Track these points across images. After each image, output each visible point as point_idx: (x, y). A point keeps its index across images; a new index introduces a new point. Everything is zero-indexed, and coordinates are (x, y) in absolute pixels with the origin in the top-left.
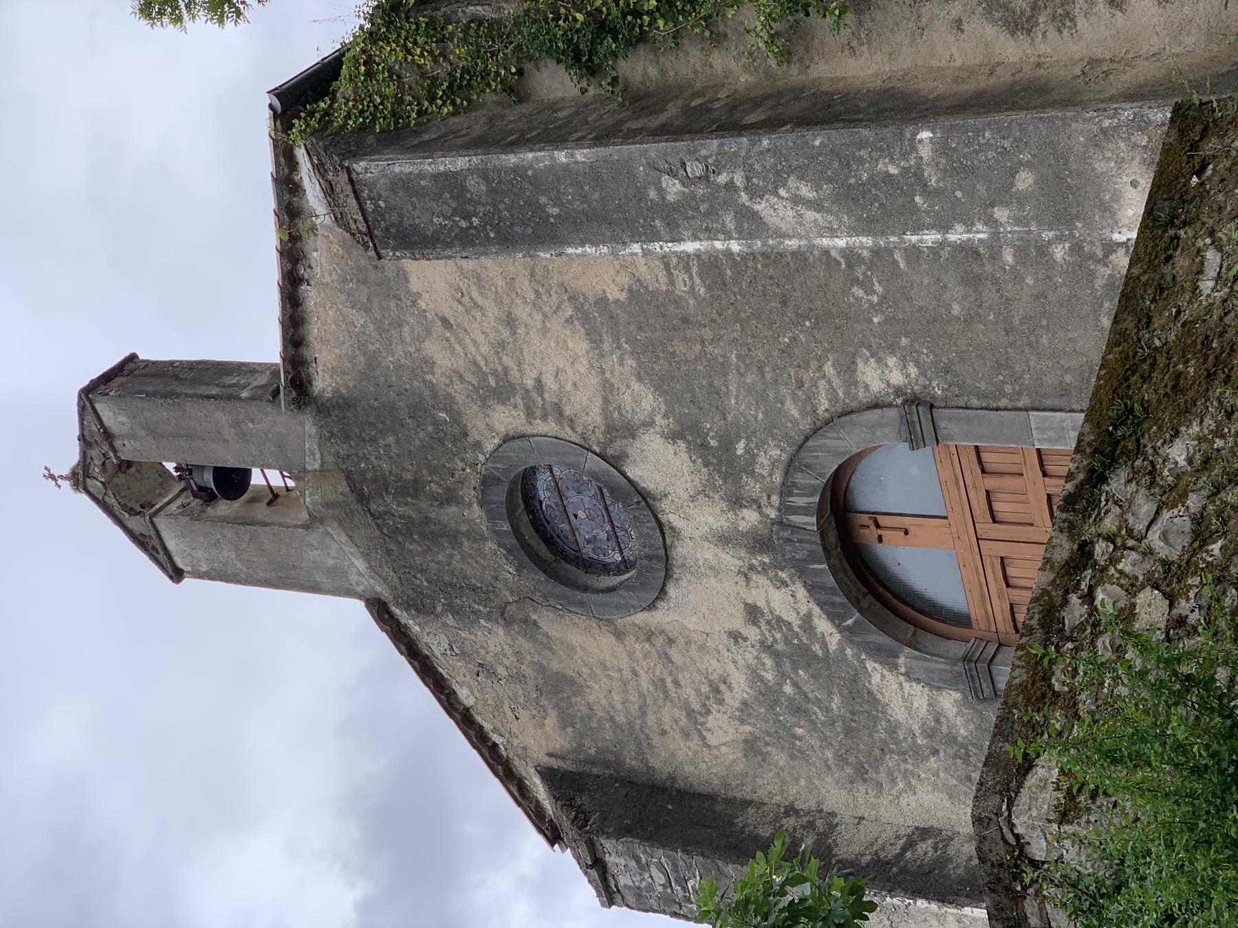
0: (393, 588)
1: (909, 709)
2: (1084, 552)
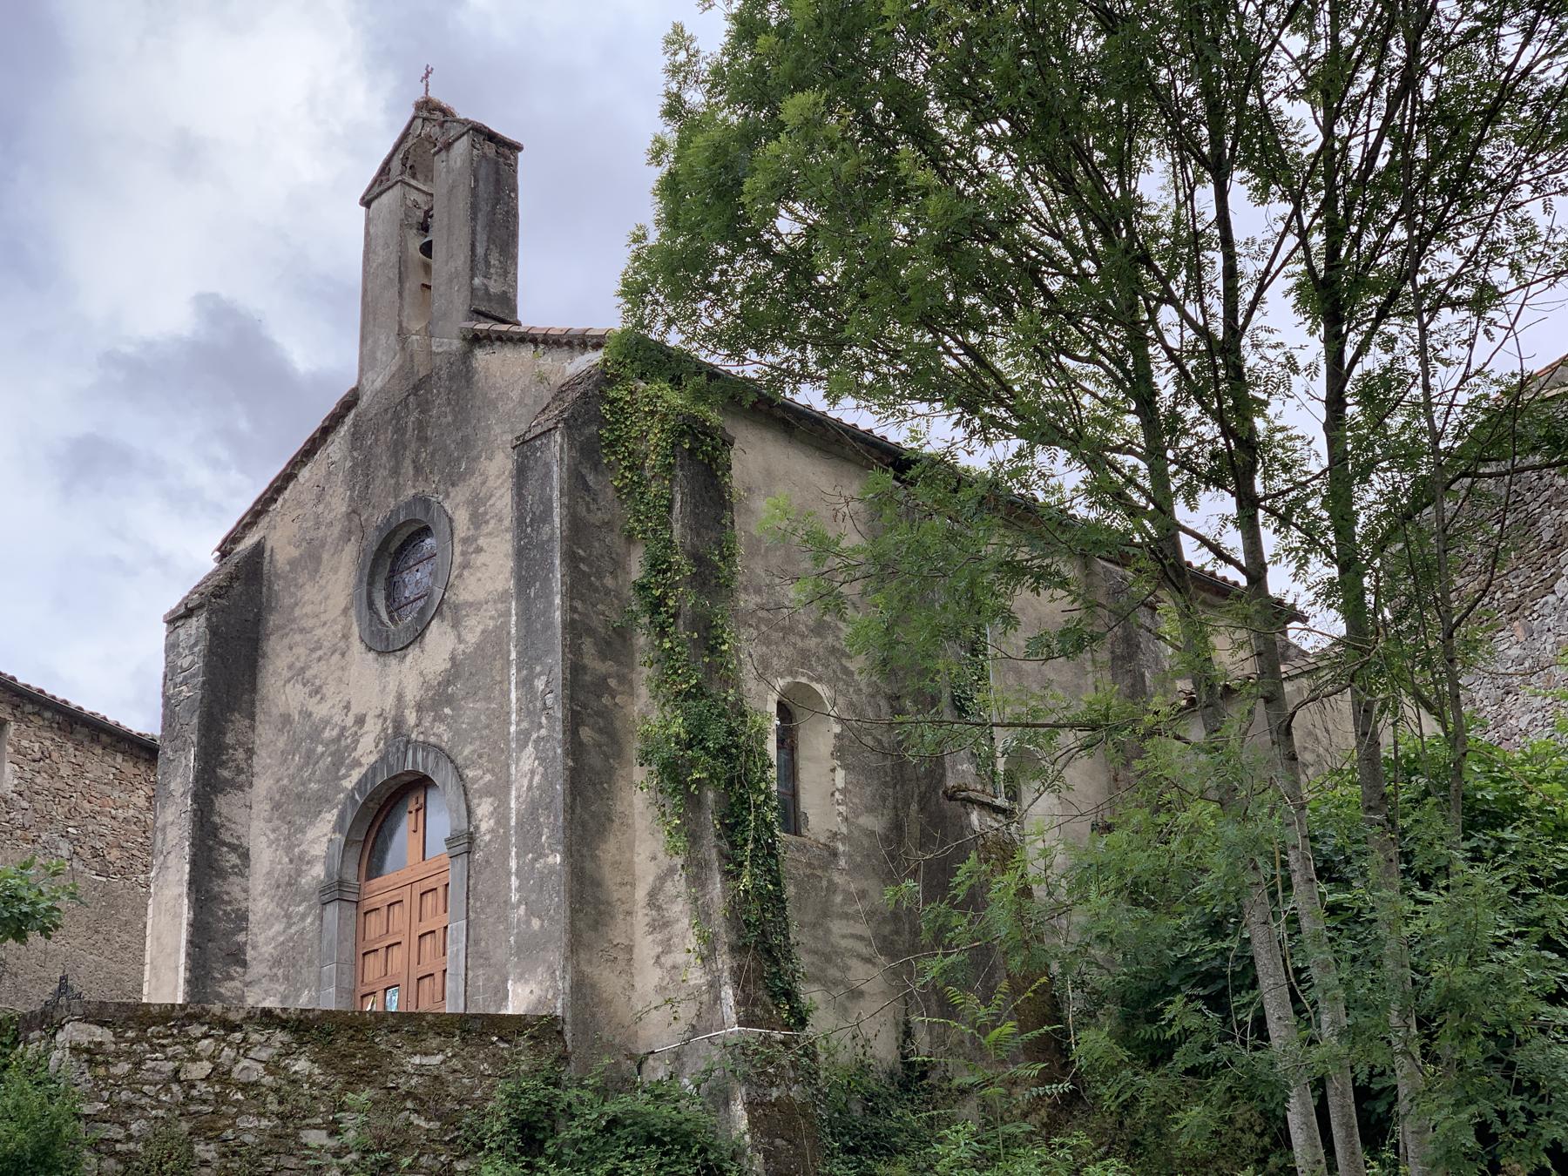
0: (366, 412)
1: (313, 842)
2: (235, 1027)
